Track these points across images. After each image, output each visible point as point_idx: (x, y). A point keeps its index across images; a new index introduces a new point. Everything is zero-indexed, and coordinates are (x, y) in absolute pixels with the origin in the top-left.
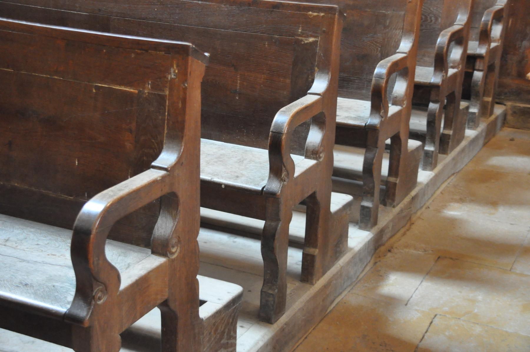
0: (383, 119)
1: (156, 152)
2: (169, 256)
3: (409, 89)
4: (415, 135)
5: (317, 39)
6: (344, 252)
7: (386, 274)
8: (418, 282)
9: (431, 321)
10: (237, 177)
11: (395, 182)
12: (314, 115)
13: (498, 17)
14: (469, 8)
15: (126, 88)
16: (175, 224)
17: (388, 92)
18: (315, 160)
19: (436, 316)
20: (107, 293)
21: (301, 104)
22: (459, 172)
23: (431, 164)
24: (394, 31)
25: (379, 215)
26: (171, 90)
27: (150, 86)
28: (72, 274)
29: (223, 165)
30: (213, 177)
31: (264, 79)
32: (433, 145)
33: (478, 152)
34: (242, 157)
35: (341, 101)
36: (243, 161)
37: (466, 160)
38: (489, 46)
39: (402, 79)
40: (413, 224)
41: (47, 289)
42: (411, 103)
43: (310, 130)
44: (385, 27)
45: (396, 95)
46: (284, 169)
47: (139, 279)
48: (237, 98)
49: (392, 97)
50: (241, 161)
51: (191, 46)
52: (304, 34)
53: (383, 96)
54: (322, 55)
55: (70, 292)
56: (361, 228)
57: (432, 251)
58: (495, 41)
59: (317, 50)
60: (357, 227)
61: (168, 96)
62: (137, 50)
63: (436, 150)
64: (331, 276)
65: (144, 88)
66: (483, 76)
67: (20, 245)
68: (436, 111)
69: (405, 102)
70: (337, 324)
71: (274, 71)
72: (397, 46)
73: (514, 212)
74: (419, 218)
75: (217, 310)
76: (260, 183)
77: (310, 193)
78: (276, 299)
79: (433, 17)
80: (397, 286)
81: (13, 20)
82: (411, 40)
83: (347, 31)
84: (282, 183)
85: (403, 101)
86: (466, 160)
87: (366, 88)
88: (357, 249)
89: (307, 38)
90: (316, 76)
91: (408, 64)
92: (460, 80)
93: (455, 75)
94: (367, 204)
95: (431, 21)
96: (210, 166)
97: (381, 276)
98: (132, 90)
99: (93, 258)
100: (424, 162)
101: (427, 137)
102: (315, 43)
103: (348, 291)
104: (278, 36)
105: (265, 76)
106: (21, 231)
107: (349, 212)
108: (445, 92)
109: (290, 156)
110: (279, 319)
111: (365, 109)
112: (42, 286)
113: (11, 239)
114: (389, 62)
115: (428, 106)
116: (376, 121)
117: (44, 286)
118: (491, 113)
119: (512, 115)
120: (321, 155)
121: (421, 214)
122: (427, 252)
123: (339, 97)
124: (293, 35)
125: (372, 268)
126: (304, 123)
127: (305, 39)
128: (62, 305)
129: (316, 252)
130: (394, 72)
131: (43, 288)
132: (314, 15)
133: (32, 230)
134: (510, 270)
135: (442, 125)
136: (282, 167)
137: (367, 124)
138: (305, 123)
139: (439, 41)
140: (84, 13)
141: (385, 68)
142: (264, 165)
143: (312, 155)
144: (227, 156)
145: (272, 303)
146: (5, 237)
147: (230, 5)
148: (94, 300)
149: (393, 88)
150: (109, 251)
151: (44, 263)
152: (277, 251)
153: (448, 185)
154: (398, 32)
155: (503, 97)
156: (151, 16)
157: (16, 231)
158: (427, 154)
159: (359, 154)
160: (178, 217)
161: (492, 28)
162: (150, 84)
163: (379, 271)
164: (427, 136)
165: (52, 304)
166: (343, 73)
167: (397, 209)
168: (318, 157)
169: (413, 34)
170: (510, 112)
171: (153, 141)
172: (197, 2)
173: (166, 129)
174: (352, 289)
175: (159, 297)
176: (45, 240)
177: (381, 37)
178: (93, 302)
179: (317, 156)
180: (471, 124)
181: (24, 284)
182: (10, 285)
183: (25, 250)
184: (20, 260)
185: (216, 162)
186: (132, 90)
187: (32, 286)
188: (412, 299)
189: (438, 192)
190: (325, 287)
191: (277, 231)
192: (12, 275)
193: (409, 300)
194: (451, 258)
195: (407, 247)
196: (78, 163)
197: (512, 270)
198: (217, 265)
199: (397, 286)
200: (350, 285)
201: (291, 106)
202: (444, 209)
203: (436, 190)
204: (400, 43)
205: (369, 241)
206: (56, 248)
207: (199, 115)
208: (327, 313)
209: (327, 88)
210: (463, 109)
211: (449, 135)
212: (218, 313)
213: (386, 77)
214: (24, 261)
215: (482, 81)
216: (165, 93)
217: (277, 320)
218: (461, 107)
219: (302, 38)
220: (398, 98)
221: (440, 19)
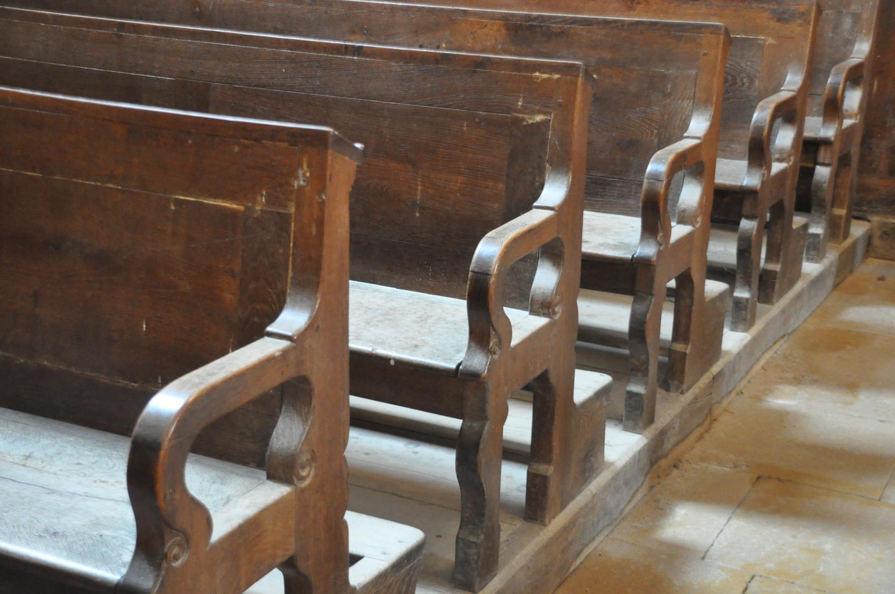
0: (662, 248)
1: (274, 308)
2: (296, 483)
3: (705, 197)
4: (717, 272)
5: (548, 118)
6: (598, 469)
7: (670, 507)
8: (724, 520)
9: (744, 586)
10: (416, 347)
11: (684, 351)
12: (543, 243)
13: (854, 77)
14: (806, 63)
15: (224, 202)
16: (307, 430)
17: (670, 202)
18: (546, 317)
19: (754, 576)
20: (188, 548)
21: (522, 226)
22: (792, 333)
23: (745, 320)
24: (680, 102)
25: (658, 407)
26: (298, 206)
27: (264, 198)
28: (129, 515)
29: (392, 327)
30: (376, 347)
31: (461, 183)
32: (747, 288)
33: (825, 298)
34: (425, 313)
35: (590, 217)
36: (426, 320)
37: (805, 313)
38: (841, 124)
39: (694, 181)
40: (715, 420)
41: (89, 542)
42: (709, 220)
43: (538, 268)
44: (666, 95)
45: (683, 206)
46: (494, 333)
47: (244, 523)
48: (417, 215)
49: (677, 211)
50: (423, 320)
51: (332, 133)
52: (527, 109)
53: (661, 210)
54: (557, 143)
55: (127, 545)
56: (626, 429)
57: (747, 466)
58: (850, 116)
59: (548, 136)
60: (621, 426)
61: (293, 215)
62: (242, 140)
63: (752, 297)
64: (576, 510)
65: (254, 203)
66: (831, 174)
67: (50, 465)
68: (752, 233)
69: (699, 219)
70: (586, 591)
71: (479, 171)
72: (685, 127)
73: (885, 401)
74: (726, 410)
75: (379, 572)
76: (453, 357)
77: (539, 372)
78: (482, 551)
79: (746, 78)
80: (688, 527)
81: (42, 93)
82: (708, 117)
83: (599, 100)
84: (490, 357)
85: (696, 217)
86: (805, 313)
87: (634, 195)
88: (620, 464)
89: (532, 115)
90: (547, 178)
91: (704, 156)
92: (791, 183)
93: (782, 174)
94: (636, 388)
95: (743, 84)
96: (372, 329)
97: (661, 509)
98: (234, 206)
99: (163, 489)
100: (733, 317)
101: (738, 276)
102: (545, 123)
103: (606, 535)
104: (484, 113)
105: (463, 178)
106: (53, 441)
107: (605, 404)
108: (767, 201)
109: (503, 309)
110: (487, 584)
111: (633, 231)
112: (81, 536)
113: (35, 454)
114: (671, 153)
115: (738, 223)
116: (649, 250)
117: (86, 536)
118: (846, 235)
119: (881, 237)
120: (557, 309)
121: (729, 403)
122: (738, 469)
123: (589, 210)
124: (509, 110)
125: (645, 495)
126: (527, 255)
127: (530, 116)
128: (112, 568)
129: (548, 470)
130: (680, 169)
131: (84, 540)
132: (543, 77)
133: (71, 439)
134: (880, 500)
135: (763, 255)
136: (489, 329)
137: (635, 256)
138: (528, 257)
139: (756, 118)
140: (167, 78)
141: (664, 163)
142: (460, 327)
143: (542, 308)
144: (399, 311)
145: (476, 558)
146: (25, 451)
147: (404, 63)
148: (167, 561)
149: (679, 195)
150: (197, 474)
151: (87, 496)
152: (483, 471)
153: (775, 355)
154: (686, 103)
155: (866, 209)
156: (275, 82)
157: (44, 442)
158: (739, 304)
159: (625, 303)
160: (311, 418)
161: (845, 95)
162: (264, 196)
163: (657, 501)
164: (738, 274)
165: (97, 567)
166: (595, 172)
167: (689, 396)
168: (551, 313)
169: (712, 106)
170: (877, 233)
171: (270, 290)
172: (351, 57)
173: (290, 271)
174: (612, 531)
175: (280, 552)
176: (90, 456)
177: (658, 112)
178: (165, 565)
179: (550, 311)
180: (812, 252)
181: (51, 533)
182: (28, 534)
183: (58, 472)
184: (48, 491)
185: (382, 321)
186: (234, 206)
187: (64, 536)
188: (712, 548)
189: (758, 367)
190: (566, 529)
191: (483, 437)
192: (33, 517)
193: (708, 550)
194: (779, 479)
195: (703, 460)
196: (146, 328)
197: (883, 500)
198: (385, 492)
199: (688, 527)
200: (608, 525)
201: (504, 229)
202: (766, 395)
203: (755, 363)
204: (690, 122)
205: (640, 452)
206: (109, 469)
207: (346, 246)
208: (567, 575)
209: (566, 198)
210: (798, 229)
211: (776, 272)
212: (382, 577)
213: (666, 178)
214: (54, 492)
215: (829, 182)
216: (289, 211)
217: (484, 587)
218: (795, 226)
219: (523, 116)
220: (687, 212)
221: (757, 81)
